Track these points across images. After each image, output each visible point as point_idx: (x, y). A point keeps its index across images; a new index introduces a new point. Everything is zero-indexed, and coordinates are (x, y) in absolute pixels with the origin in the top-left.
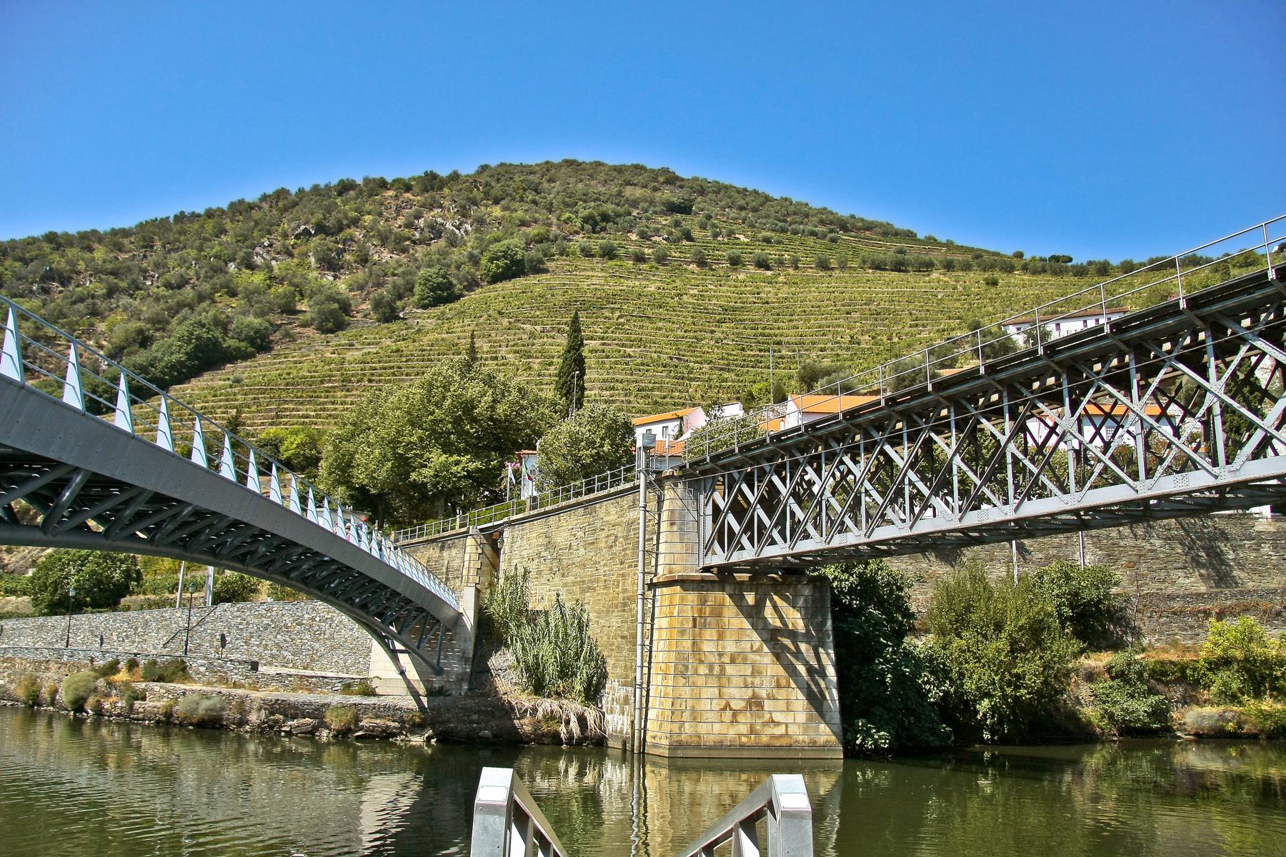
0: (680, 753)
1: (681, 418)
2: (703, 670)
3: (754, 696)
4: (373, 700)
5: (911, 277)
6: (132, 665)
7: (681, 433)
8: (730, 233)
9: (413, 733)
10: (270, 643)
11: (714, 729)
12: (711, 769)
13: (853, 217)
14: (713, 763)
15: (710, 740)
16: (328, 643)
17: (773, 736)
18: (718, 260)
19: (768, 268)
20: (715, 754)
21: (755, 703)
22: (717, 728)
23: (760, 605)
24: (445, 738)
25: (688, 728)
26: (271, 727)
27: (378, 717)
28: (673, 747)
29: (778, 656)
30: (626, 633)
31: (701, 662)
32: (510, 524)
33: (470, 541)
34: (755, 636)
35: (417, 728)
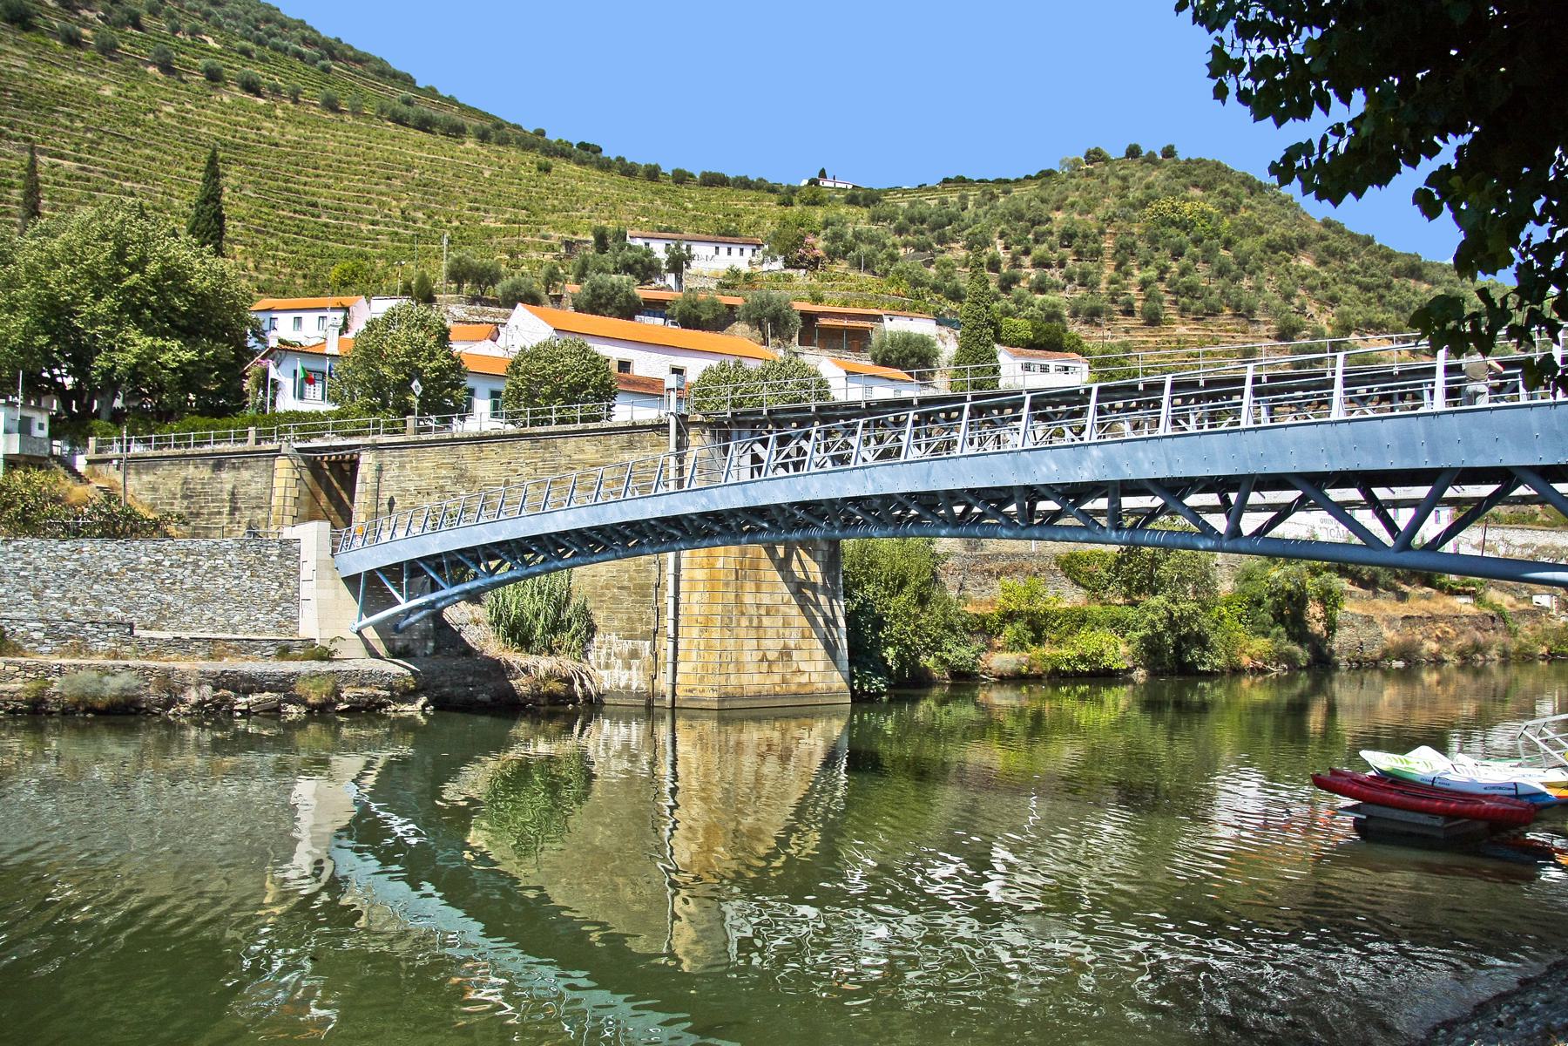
0: (727, 705)
1: (347, 309)
2: (744, 622)
3: (785, 647)
7: (345, 328)
8: (194, 32)
9: (403, 702)
10: (81, 596)
11: (754, 680)
12: (796, 717)
13: (339, 40)
14: (755, 713)
16: (192, 595)
17: (800, 684)
18: (189, 67)
19: (259, 95)
20: (756, 704)
21: (786, 653)
22: (757, 678)
23: (788, 558)
24: (442, 705)
25: (733, 680)
26: (218, 707)
27: (363, 685)
28: (721, 699)
29: (802, 608)
30: (626, 584)
31: (743, 614)
32: (375, 447)
34: (785, 589)
35: (408, 695)
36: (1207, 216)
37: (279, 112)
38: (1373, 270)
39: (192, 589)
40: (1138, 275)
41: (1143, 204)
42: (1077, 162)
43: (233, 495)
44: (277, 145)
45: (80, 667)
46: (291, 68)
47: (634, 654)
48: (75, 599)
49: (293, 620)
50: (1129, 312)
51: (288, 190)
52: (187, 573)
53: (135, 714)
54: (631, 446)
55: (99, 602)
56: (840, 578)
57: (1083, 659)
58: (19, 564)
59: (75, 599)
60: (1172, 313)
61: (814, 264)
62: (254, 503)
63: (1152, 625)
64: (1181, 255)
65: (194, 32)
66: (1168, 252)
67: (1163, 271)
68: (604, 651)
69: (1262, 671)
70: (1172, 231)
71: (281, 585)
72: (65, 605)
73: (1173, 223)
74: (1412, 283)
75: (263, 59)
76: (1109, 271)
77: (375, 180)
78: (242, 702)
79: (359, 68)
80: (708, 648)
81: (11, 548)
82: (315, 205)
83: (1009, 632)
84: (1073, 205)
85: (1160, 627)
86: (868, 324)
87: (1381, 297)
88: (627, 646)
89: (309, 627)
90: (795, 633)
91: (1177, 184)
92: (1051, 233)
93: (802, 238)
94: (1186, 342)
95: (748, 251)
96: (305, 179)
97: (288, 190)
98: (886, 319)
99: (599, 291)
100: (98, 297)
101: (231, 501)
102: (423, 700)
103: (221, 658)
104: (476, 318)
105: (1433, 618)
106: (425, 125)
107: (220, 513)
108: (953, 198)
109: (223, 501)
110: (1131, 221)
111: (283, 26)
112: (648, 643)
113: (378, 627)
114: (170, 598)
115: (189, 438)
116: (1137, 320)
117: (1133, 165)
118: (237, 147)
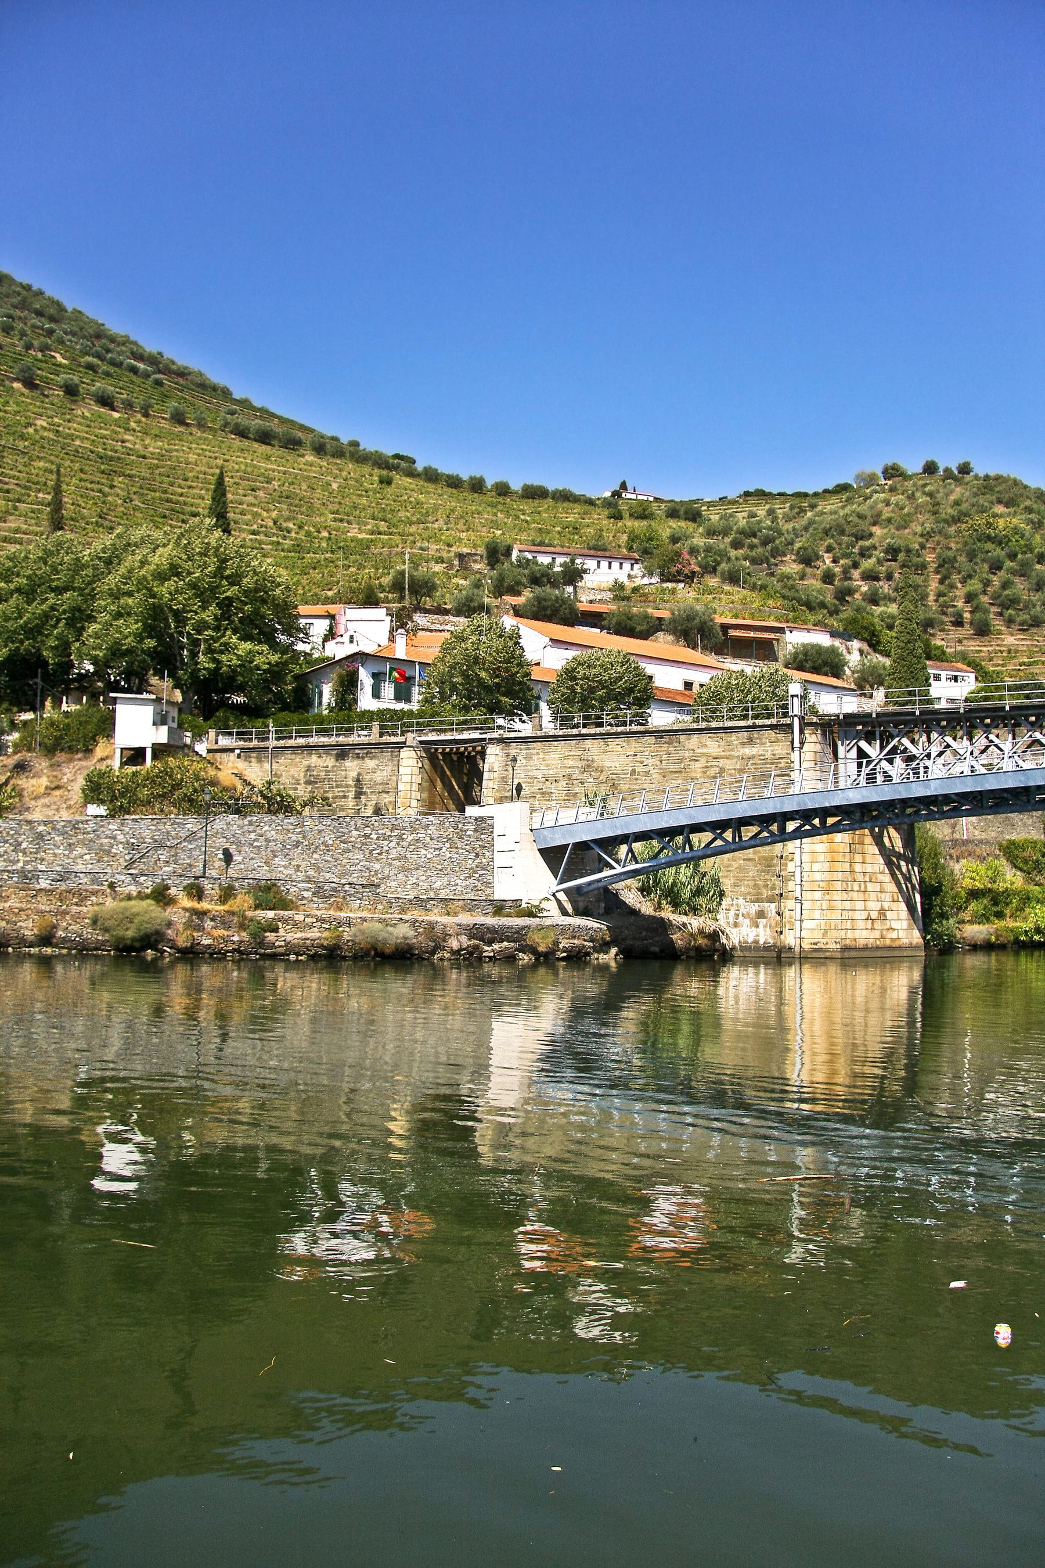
0: (846, 955)
3: (882, 909)
4: (537, 921)
5: (275, 451)
6: (196, 892)
10: (303, 864)
11: (864, 936)
15: (861, 943)
16: (396, 863)
19: (113, 410)
21: (882, 912)
22: (865, 934)
24: (628, 954)
26: (471, 954)
27: (574, 937)
33: (405, 753)
35: (604, 947)
36: (1016, 530)
37: (133, 425)
39: (398, 859)
40: (961, 591)
41: (956, 520)
43: (358, 781)
44: (144, 457)
45: (365, 920)
46: (132, 382)
47: (761, 914)
48: (298, 866)
49: (489, 884)
50: (959, 623)
51: (168, 501)
52: (392, 845)
53: (409, 959)
54: (750, 741)
55: (319, 870)
56: (913, 851)
58: (253, 836)
59: (298, 866)
60: (997, 624)
61: (689, 578)
62: (381, 788)
64: (1000, 568)
65: (44, 348)
66: (986, 567)
67: (987, 583)
68: (732, 913)
70: (989, 546)
71: (477, 855)
72: (290, 871)
73: (989, 538)
75: (108, 374)
76: (934, 585)
77: (241, 492)
78: (488, 950)
79: (181, 381)
80: (831, 909)
81: (246, 822)
83: (973, 906)
84: (889, 520)
86: (772, 636)
88: (755, 908)
89: (503, 889)
90: (887, 897)
91: (982, 500)
92: (875, 548)
94: (1016, 652)
95: (627, 566)
96: (180, 490)
97: (168, 501)
98: (788, 632)
99: (544, 603)
100: (204, 608)
101: (356, 786)
102: (614, 951)
103: (456, 914)
104: (438, 627)
106: (265, 438)
107: (345, 797)
108: (761, 512)
109: (347, 786)
110: (947, 537)
111: (113, 340)
112: (773, 905)
113: (566, 891)
114: (377, 866)
115: (251, 733)
116: (967, 630)
118: (111, 459)
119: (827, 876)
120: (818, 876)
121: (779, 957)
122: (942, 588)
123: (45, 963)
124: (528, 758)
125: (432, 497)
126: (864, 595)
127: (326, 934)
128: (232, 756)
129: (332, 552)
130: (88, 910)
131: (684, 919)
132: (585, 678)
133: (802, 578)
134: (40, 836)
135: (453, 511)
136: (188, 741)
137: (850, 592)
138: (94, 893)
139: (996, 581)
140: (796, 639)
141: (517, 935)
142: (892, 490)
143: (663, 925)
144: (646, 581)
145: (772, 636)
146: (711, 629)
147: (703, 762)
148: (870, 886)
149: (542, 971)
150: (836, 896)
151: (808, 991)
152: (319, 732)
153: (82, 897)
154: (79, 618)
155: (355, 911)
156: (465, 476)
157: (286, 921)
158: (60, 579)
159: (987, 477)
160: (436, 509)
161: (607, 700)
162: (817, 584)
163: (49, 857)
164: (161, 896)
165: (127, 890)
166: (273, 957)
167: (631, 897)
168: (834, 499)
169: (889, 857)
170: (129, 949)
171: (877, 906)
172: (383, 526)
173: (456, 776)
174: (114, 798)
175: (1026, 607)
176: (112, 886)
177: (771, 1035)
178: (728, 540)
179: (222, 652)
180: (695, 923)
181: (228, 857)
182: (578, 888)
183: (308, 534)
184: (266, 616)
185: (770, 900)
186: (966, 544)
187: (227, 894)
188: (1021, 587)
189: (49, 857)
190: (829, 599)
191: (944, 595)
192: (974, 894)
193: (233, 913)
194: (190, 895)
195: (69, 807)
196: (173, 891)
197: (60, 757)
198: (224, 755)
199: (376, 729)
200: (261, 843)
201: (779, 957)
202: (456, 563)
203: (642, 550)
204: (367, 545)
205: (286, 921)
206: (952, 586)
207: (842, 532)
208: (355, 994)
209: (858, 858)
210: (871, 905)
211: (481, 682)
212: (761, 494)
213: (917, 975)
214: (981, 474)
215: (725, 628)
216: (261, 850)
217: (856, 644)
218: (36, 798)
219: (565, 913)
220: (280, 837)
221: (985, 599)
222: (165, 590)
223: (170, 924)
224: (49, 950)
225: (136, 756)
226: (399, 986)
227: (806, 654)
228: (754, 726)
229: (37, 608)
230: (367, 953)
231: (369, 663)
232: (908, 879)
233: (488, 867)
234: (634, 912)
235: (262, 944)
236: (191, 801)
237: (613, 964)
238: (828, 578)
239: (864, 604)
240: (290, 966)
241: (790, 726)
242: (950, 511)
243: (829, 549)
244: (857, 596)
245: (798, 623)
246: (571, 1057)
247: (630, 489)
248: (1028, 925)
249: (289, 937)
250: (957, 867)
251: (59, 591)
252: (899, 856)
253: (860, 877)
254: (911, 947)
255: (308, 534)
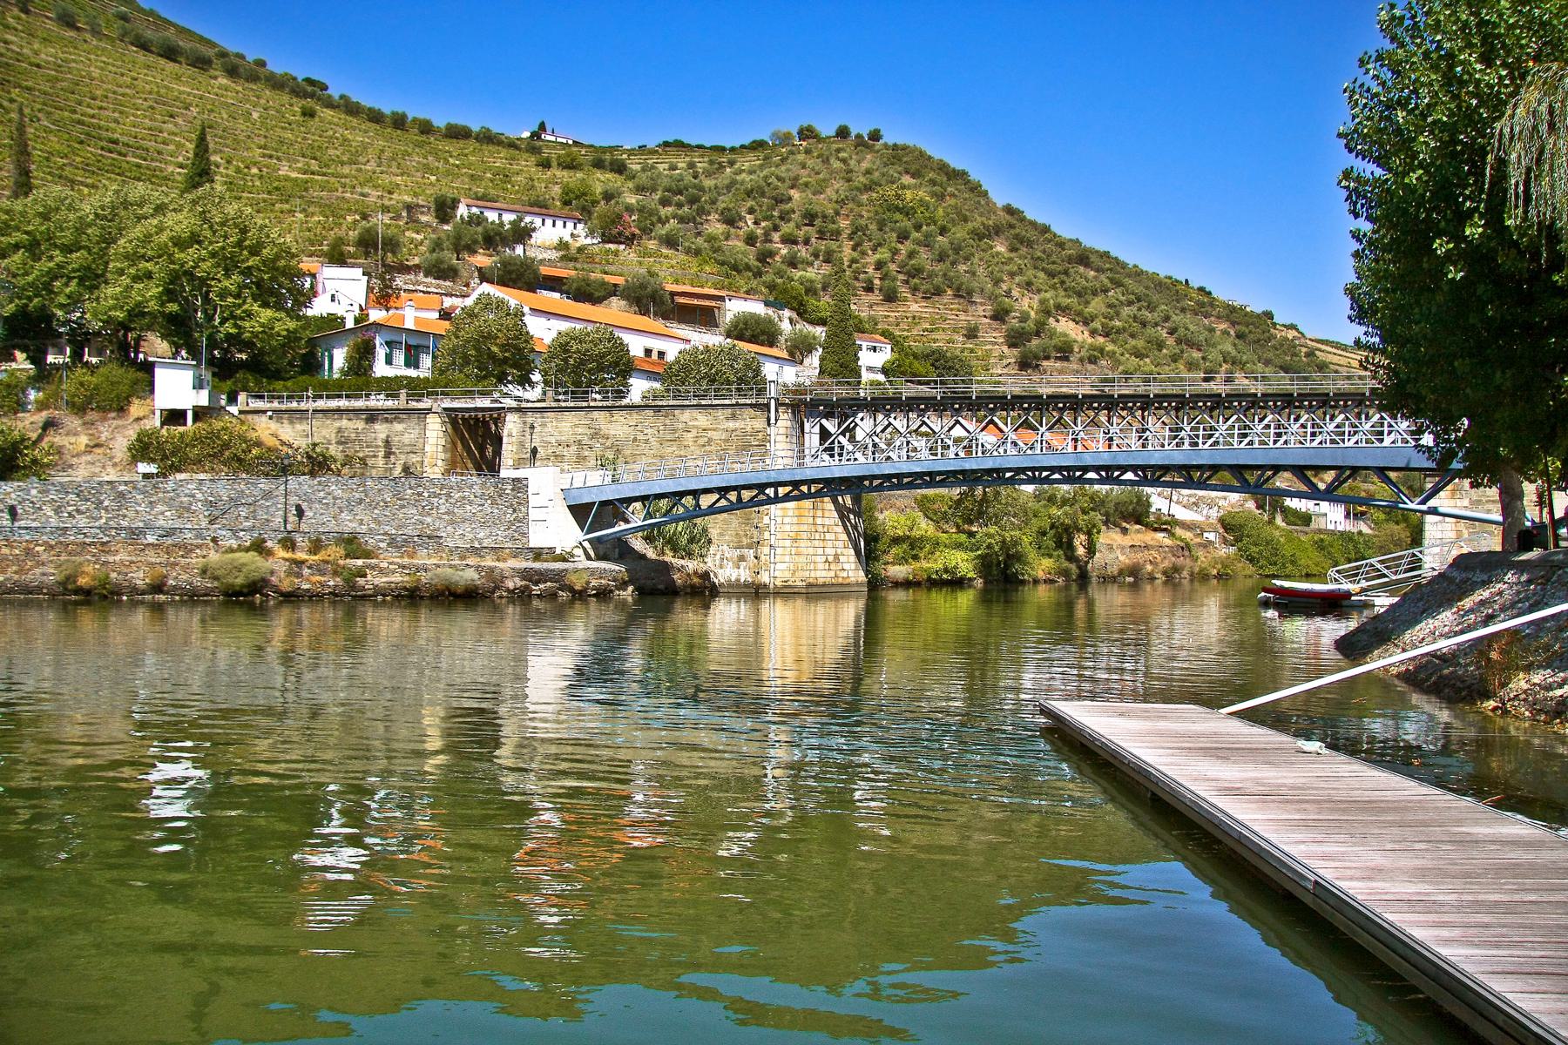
10: (366, 519)
11: (822, 575)
15: (821, 581)
21: (836, 556)
24: (642, 592)
35: (623, 585)
38: (1054, 258)
40: (872, 258)
42: (788, 136)
43: (387, 442)
44: (38, 66)
47: (742, 558)
51: (80, 122)
54: (734, 417)
55: (379, 523)
57: (946, 570)
58: (322, 494)
60: (904, 291)
61: (630, 240)
62: (409, 449)
63: (989, 546)
64: (906, 238)
67: (895, 252)
69: (1052, 582)
70: (898, 216)
73: (898, 209)
74: (1081, 269)
78: (536, 590)
82: (116, 142)
84: (806, 185)
85: (997, 548)
86: (713, 304)
87: (1063, 282)
89: (537, 539)
90: (840, 544)
91: (892, 171)
93: (620, 217)
96: (92, 112)
97: (80, 122)
102: (630, 588)
104: (411, 287)
105: (1147, 547)
106: (171, 53)
113: (589, 540)
114: (429, 520)
116: (876, 297)
117: (847, 146)
119: (795, 528)
120: (787, 528)
121: (757, 593)
122: (855, 254)
123: (158, 609)
124: (543, 425)
125: (358, 134)
126: (784, 257)
127: (407, 578)
128: (264, 418)
129: (269, 193)
130: (195, 561)
131: (682, 562)
132: (578, 351)
133: (727, 239)
134: (122, 495)
135: (382, 151)
136: (223, 403)
137: (771, 254)
138: (199, 547)
139: (904, 249)
140: (735, 308)
141: (558, 576)
142: (808, 152)
143: (666, 568)
144: (589, 241)
145: (713, 304)
146: (661, 297)
147: (694, 433)
148: (828, 536)
149: (578, 605)
150: (803, 543)
151: (779, 618)
152: (347, 396)
153: (188, 549)
154: (92, 278)
155: (424, 558)
156: (387, 110)
157: (373, 568)
158: (66, 237)
159: (895, 147)
160: (365, 147)
161: (591, 372)
162: (740, 245)
163: (131, 514)
164: (259, 547)
165: (228, 544)
166: (363, 597)
167: (638, 544)
168: (751, 156)
169: (842, 513)
170: (238, 594)
171: (832, 551)
172: (314, 165)
173: (477, 441)
174: (165, 457)
175: (930, 276)
176: (214, 540)
177: (751, 648)
178: (657, 196)
179: (242, 319)
180: (691, 565)
181: (300, 513)
182: (599, 539)
183: (238, 171)
184: (282, 285)
185: (749, 547)
186: (877, 213)
187: (316, 546)
188: (924, 256)
189: (131, 514)
190: (754, 263)
191: (856, 261)
192: (896, 540)
193: (327, 562)
194: (286, 548)
195: (115, 465)
196: (269, 544)
197: (92, 416)
198: (256, 417)
199: (403, 396)
200: (329, 500)
201: (757, 593)
202: (404, 214)
203: (576, 205)
204: (305, 186)
205: (373, 568)
206: (864, 253)
207: (763, 194)
208: (428, 625)
209: (819, 513)
210: (828, 551)
211: (492, 356)
212: (679, 145)
213: (862, 603)
214: (890, 143)
215: (673, 294)
216: (330, 508)
217: (787, 313)
218: (78, 455)
219: (589, 558)
220: (346, 496)
221: (893, 267)
222: (189, 256)
223: (272, 573)
224: (162, 597)
225: (174, 417)
226: (466, 622)
227: (746, 324)
228: (737, 404)
229: (44, 265)
230: (441, 593)
231: (383, 331)
232: (855, 527)
233: (524, 520)
234: (643, 557)
235: (354, 587)
236: (239, 460)
237: (630, 599)
238: (750, 240)
239: (784, 267)
240: (376, 605)
241: (768, 406)
242: (862, 179)
243: (751, 211)
244: (777, 258)
245: (735, 292)
246: (597, 670)
247: (549, 130)
248: (939, 566)
249: (377, 581)
250: (881, 517)
251: (68, 249)
252: (850, 511)
253: (820, 529)
254: (858, 584)
255: (238, 171)
